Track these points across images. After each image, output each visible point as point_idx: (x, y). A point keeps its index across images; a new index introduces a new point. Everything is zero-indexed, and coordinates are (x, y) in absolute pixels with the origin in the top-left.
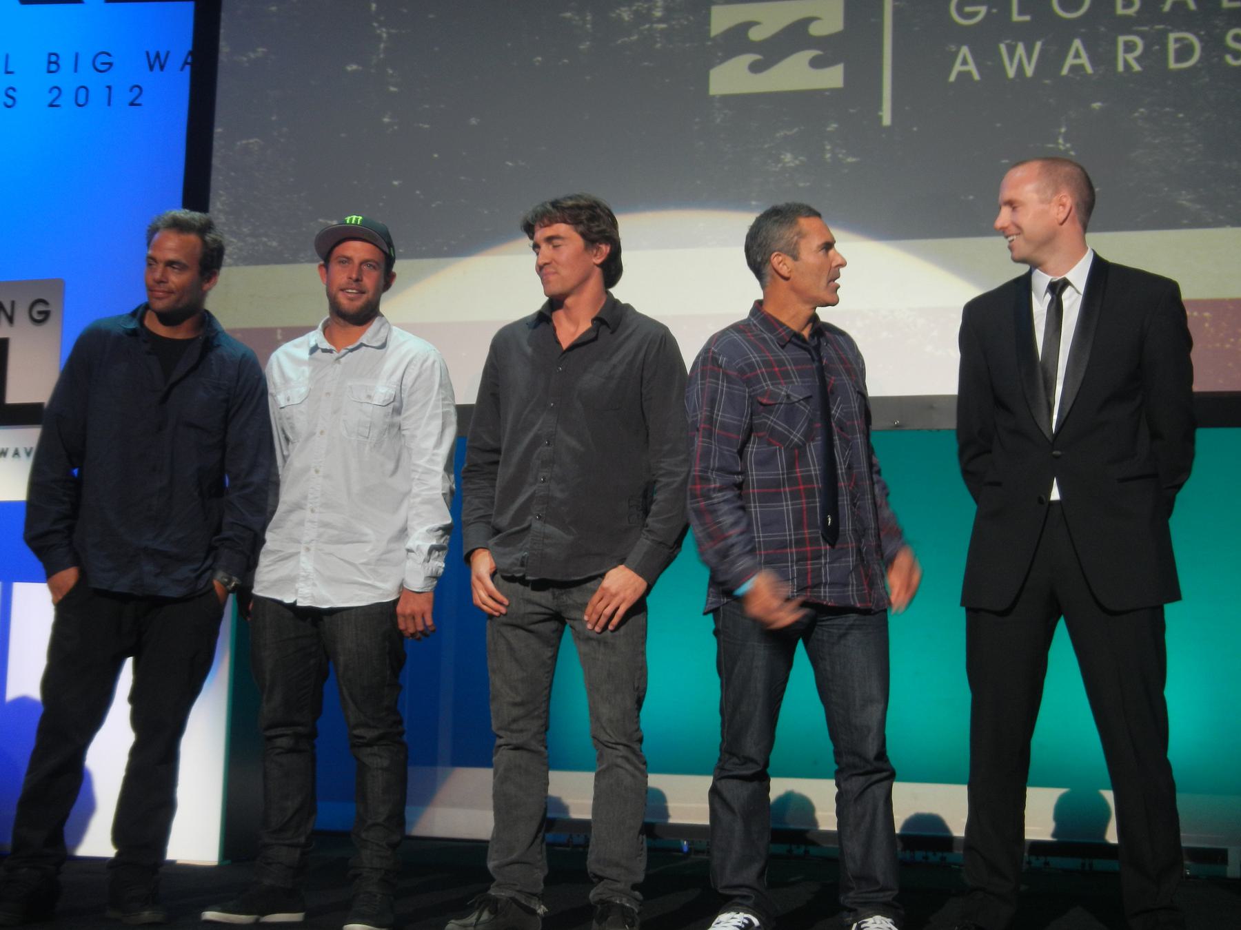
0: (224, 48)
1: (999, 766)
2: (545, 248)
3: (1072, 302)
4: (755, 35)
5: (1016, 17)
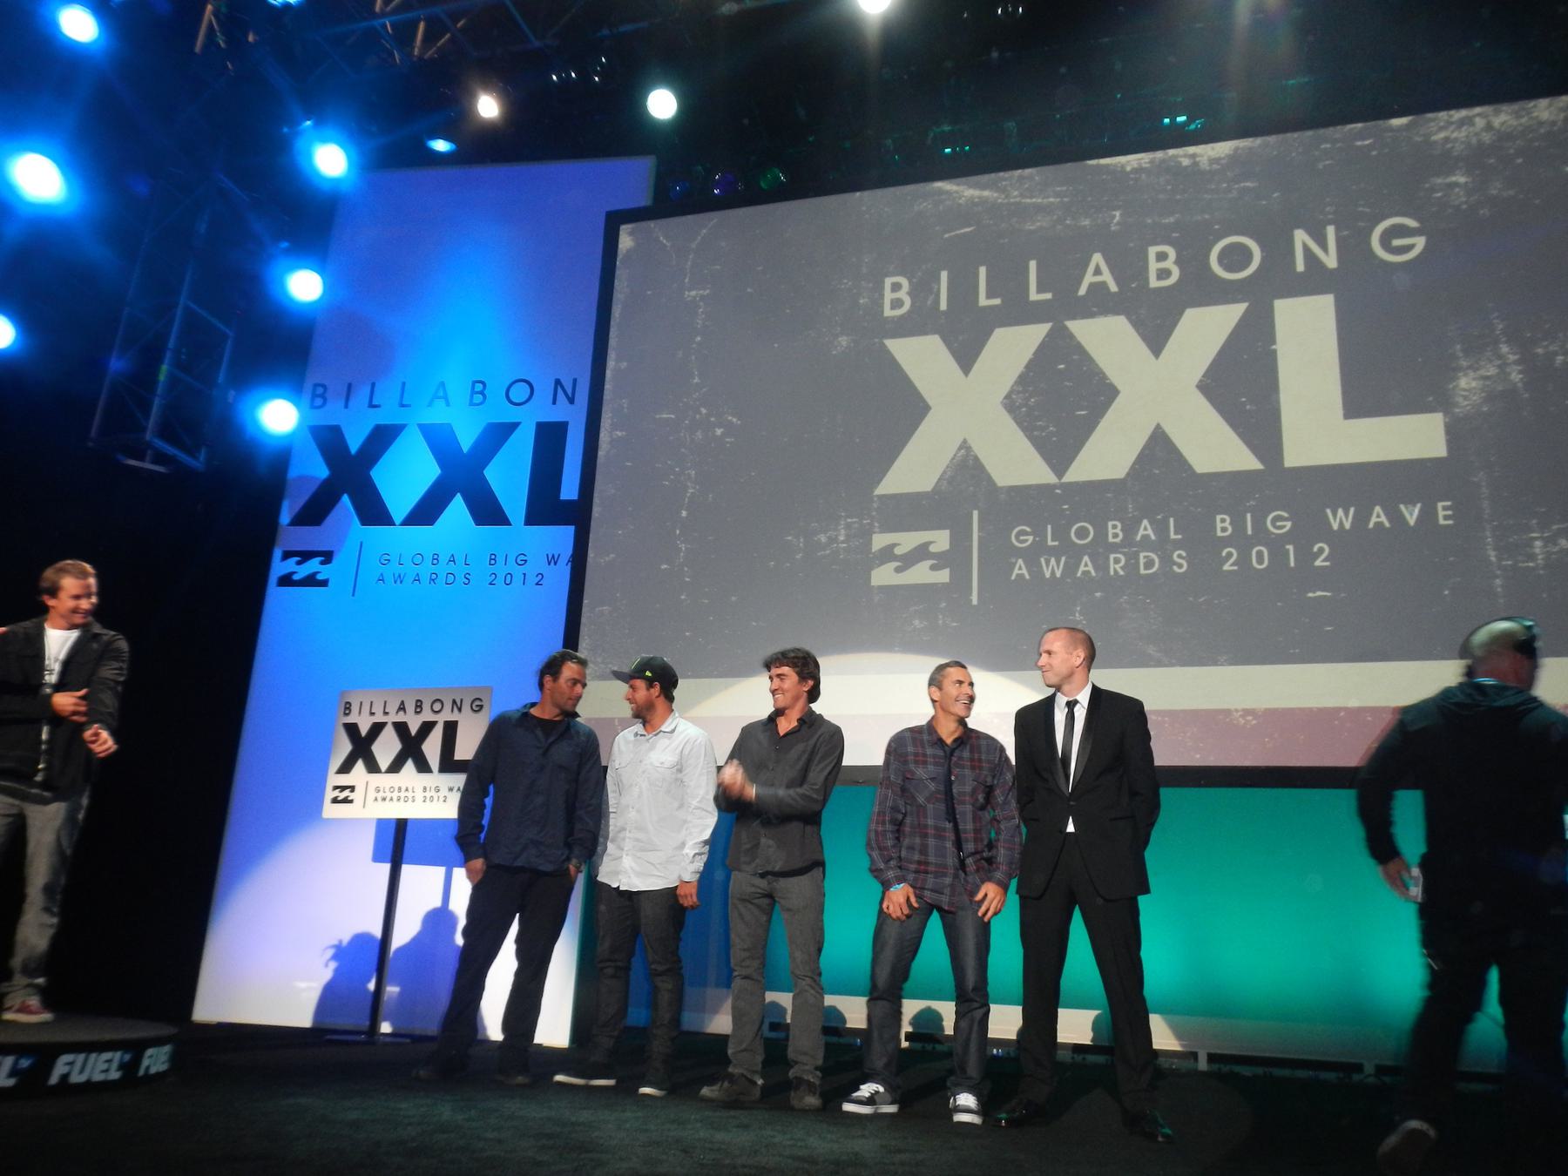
0: (591, 554)
1: (1041, 999)
2: (776, 680)
3: (1080, 714)
4: (898, 551)
5: (1050, 543)
